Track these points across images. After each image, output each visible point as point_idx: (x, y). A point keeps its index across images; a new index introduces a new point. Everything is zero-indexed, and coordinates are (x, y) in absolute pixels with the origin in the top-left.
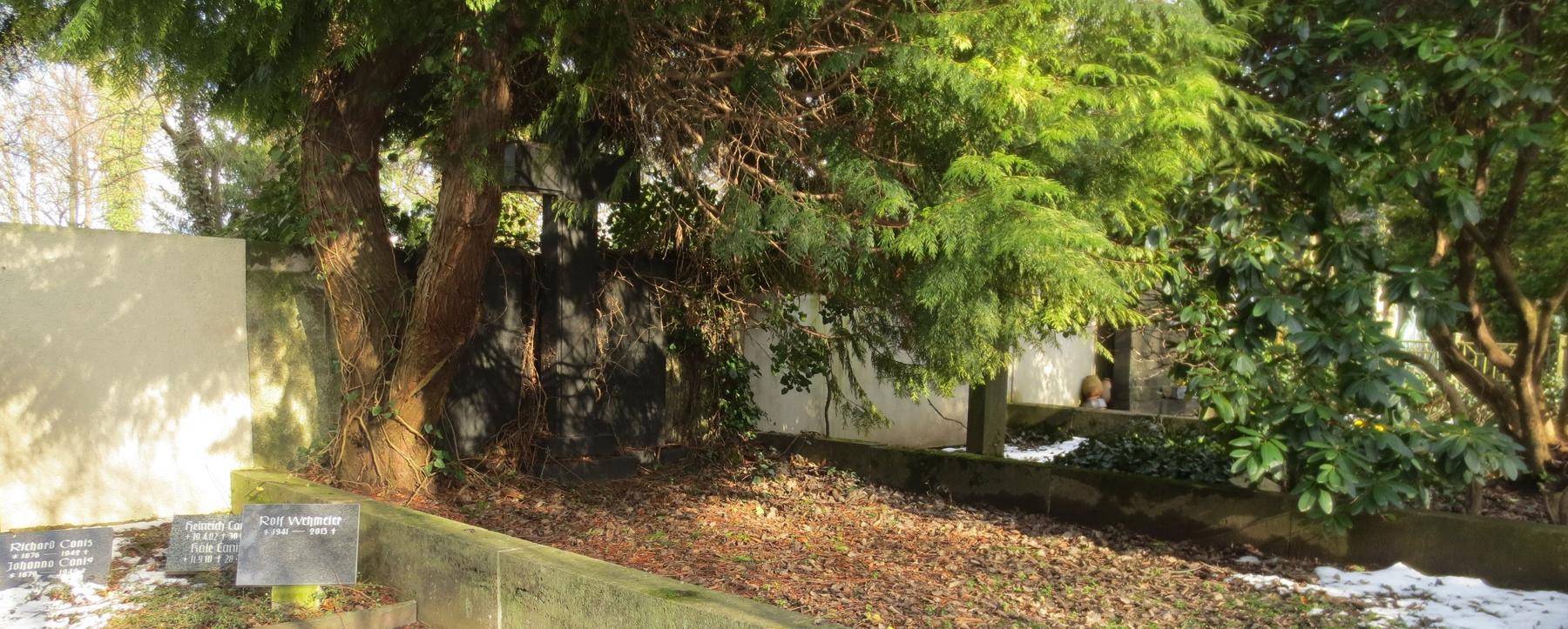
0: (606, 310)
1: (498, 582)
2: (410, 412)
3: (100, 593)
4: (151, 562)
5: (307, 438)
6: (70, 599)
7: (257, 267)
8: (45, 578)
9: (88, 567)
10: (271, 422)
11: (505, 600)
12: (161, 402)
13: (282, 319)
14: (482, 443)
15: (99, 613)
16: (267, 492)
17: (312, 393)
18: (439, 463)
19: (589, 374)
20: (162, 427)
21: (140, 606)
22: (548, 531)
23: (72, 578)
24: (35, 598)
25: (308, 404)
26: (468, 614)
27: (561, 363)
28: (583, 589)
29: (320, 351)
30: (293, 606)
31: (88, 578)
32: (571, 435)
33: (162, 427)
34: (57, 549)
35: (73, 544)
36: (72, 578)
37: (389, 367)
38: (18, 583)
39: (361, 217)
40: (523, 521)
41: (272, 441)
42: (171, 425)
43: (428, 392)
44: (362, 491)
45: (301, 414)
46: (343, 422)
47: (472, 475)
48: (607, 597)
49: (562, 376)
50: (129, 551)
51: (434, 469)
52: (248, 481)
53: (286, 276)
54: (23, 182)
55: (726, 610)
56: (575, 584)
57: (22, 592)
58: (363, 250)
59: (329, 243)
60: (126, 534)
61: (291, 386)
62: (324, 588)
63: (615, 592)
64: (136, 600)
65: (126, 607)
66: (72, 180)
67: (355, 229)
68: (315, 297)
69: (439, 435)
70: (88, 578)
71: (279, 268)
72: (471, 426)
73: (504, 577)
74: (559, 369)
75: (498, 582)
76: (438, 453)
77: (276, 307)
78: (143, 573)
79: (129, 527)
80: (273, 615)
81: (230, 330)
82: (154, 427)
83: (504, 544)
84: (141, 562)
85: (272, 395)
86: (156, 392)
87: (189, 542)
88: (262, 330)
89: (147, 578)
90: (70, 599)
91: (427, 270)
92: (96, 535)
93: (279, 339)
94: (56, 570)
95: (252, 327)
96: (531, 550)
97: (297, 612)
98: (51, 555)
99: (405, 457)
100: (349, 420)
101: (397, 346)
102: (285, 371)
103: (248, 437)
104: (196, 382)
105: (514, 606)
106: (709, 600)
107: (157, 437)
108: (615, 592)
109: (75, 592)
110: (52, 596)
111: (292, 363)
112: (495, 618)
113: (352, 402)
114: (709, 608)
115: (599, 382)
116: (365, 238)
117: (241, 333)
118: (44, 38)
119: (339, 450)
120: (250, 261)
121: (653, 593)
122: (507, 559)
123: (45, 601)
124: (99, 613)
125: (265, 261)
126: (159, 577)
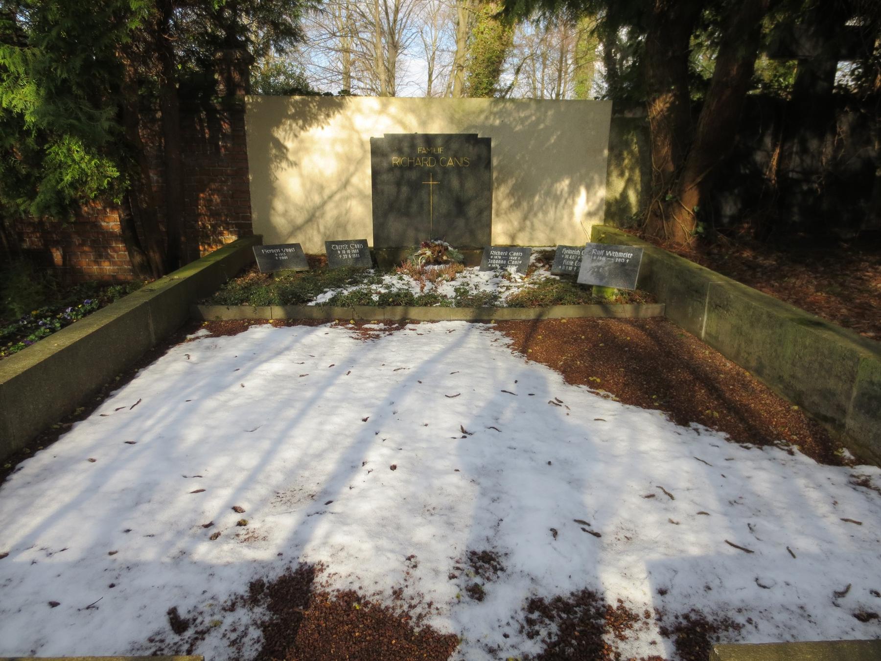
0: (834, 133)
1: (707, 300)
2: (691, 201)
3: (521, 278)
4: (547, 266)
5: (634, 210)
6: (509, 279)
7: (617, 115)
8: (501, 268)
9: (519, 265)
10: (616, 201)
11: (709, 311)
12: (566, 189)
13: (627, 145)
14: (736, 219)
15: (518, 287)
16: (606, 238)
17: (639, 187)
18: (700, 229)
19: (814, 177)
20: (566, 202)
21: (536, 287)
22: (759, 275)
23: (512, 269)
24: (497, 277)
25: (636, 190)
26: (690, 315)
27: (793, 171)
28: (752, 310)
29: (643, 162)
30: (602, 297)
31: (518, 271)
32: (796, 218)
33: (566, 202)
34: (508, 256)
35: (515, 254)
36: (512, 269)
37: (680, 171)
38: (491, 269)
39: (673, 84)
40: (745, 268)
41: (615, 210)
42: (570, 201)
43: (701, 186)
44: (655, 242)
45: (633, 197)
46: (650, 202)
47: (723, 238)
48: (764, 317)
49: (792, 179)
50: (538, 260)
51: (697, 233)
52: (599, 231)
53: (633, 120)
54: (539, 75)
55: (837, 337)
56: (748, 307)
57: (492, 273)
58: (672, 104)
59: (654, 100)
60: (541, 252)
61: (629, 181)
62: (619, 290)
63: (770, 316)
64: (535, 283)
65: (531, 286)
66: (560, 71)
67: (669, 91)
68: (644, 130)
69: (706, 214)
70: (518, 271)
71: (628, 115)
72: (729, 209)
73: (711, 298)
74: (790, 175)
75: (707, 300)
76: (701, 224)
77: (625, 137)
78: (542, 271)
79: (542, 249)
80: (590, 300)
81: (602, 151)
82: (562, 202)
83: (717, 278)
84: (543, 266)
85: (619, 185)
86: (564, 184)
87: (564, 259)
88: (617, 150)
89: (543, 274)
90: (509, 279)
91: (704, 113)
92: (526, 252)
93: (625, 153)
94: (506, 265)
95: (611, 149)
96: (731, 284)
97: (604, 300)
98: (506, 258)
99: (684, 225)
100: (654, 201)
101: (685, 160)
102: (627, 174)
103: (604, 207)
104: (581, 181)
105: (713, 315)
106: (830, 329)
107: (563, 208)
108: (770, 316)
109: (512, 276)
110: (503, 277)
111: (632, 169)
112: (702, 320)
113: (659, 192)
114: (826, 334)
115: (820, 184)
116: (675, 95)
117: (606, 152)
118: (299, 77)
119: (646, 218)
120: (614, 112)
121: (792, 320)
122: (715, 287)
123: (500, 278)
124: (518, 287)
125: (621, 112)
126: (547, 274)
